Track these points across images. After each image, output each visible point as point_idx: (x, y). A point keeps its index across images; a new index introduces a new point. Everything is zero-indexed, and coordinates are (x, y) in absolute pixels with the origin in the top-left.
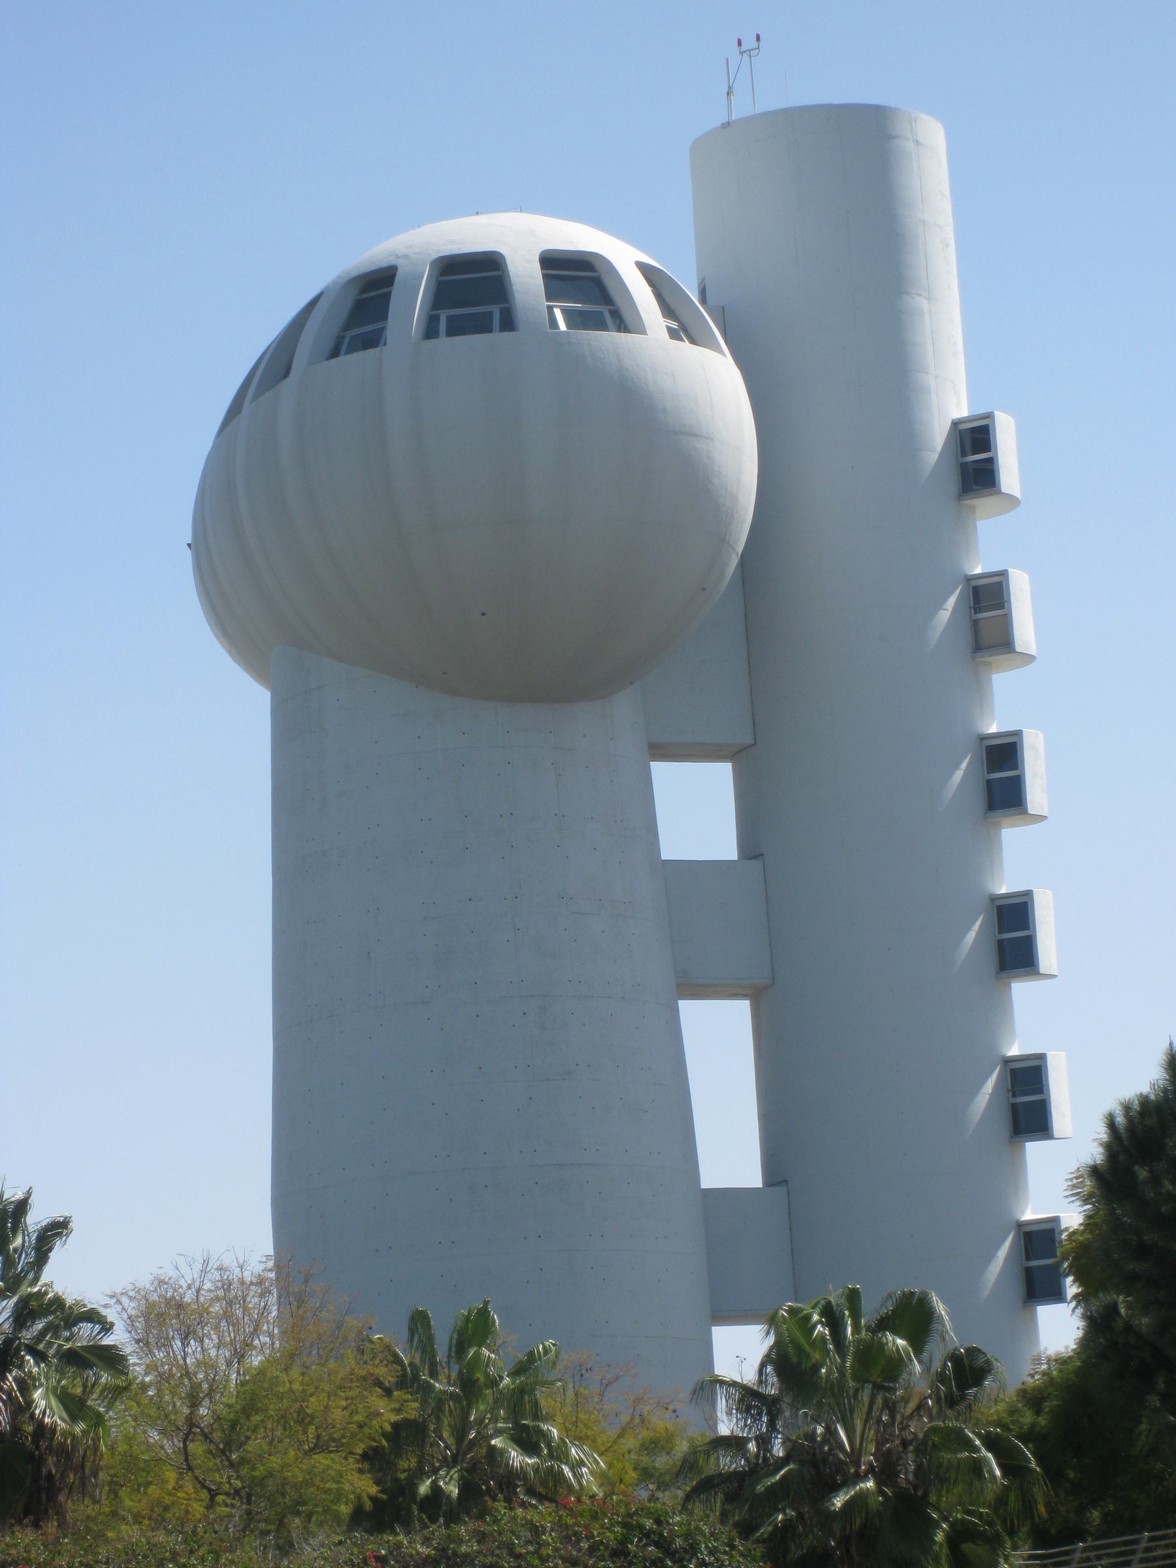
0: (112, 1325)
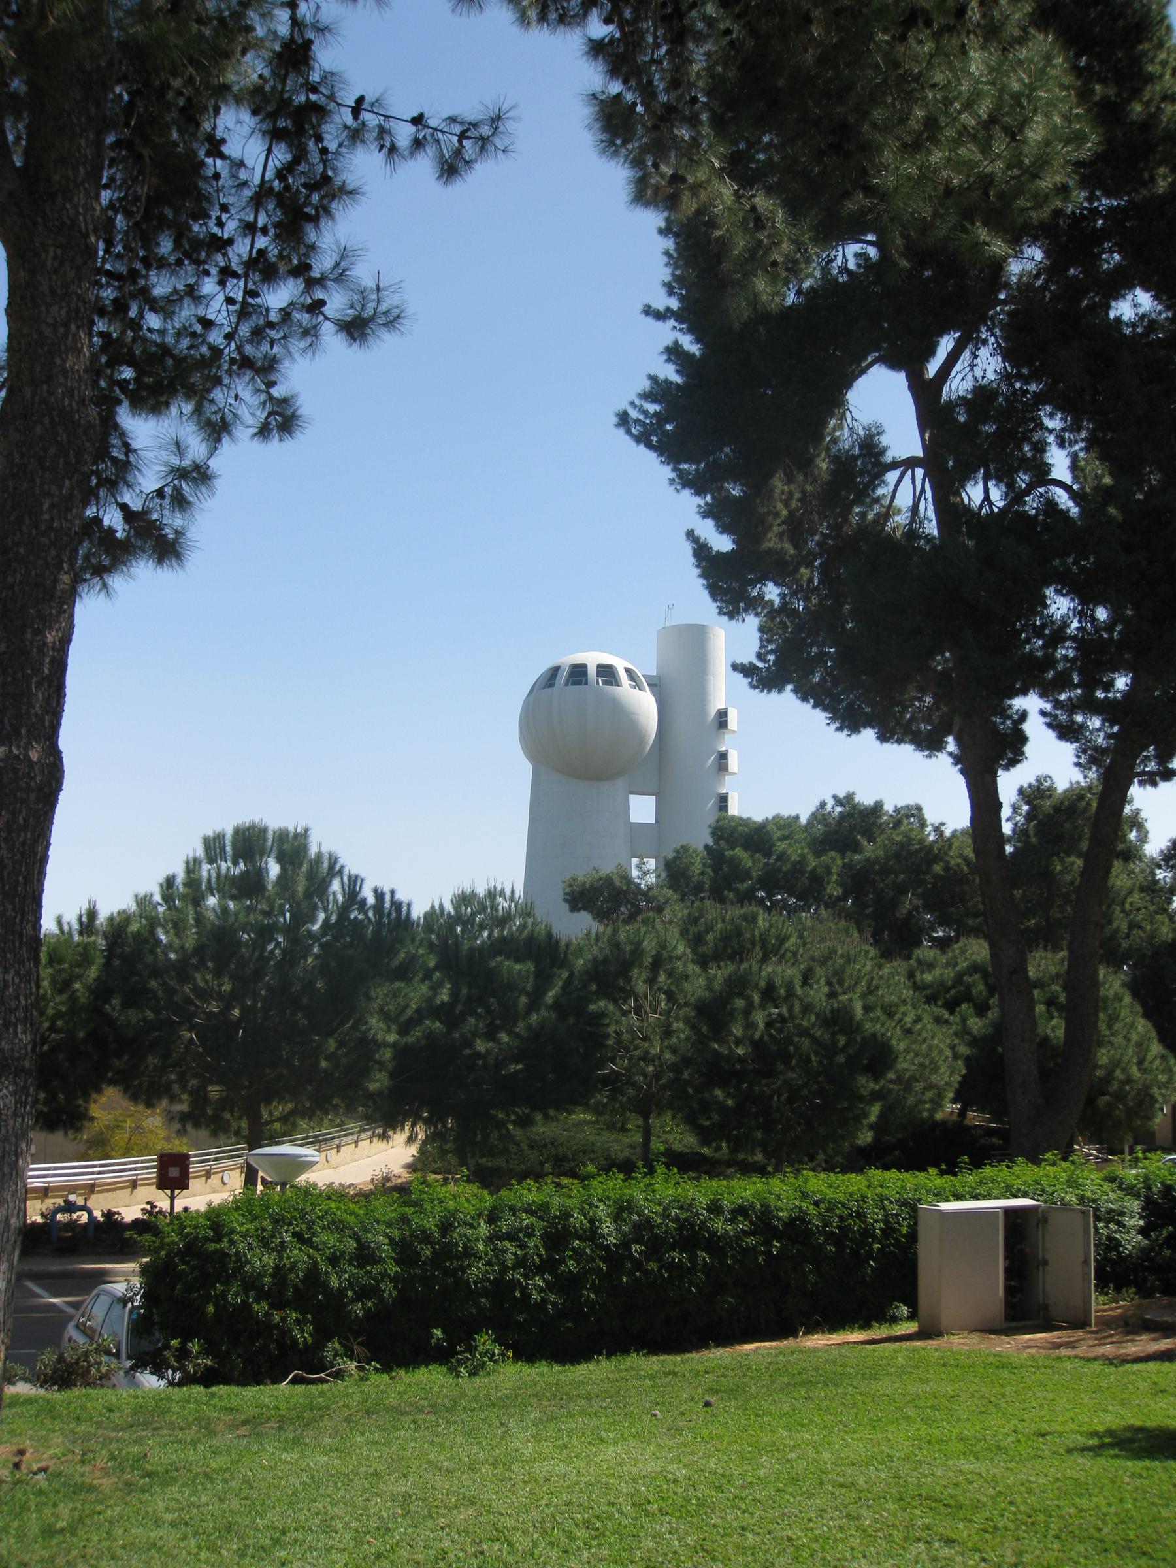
0: (574, 908)
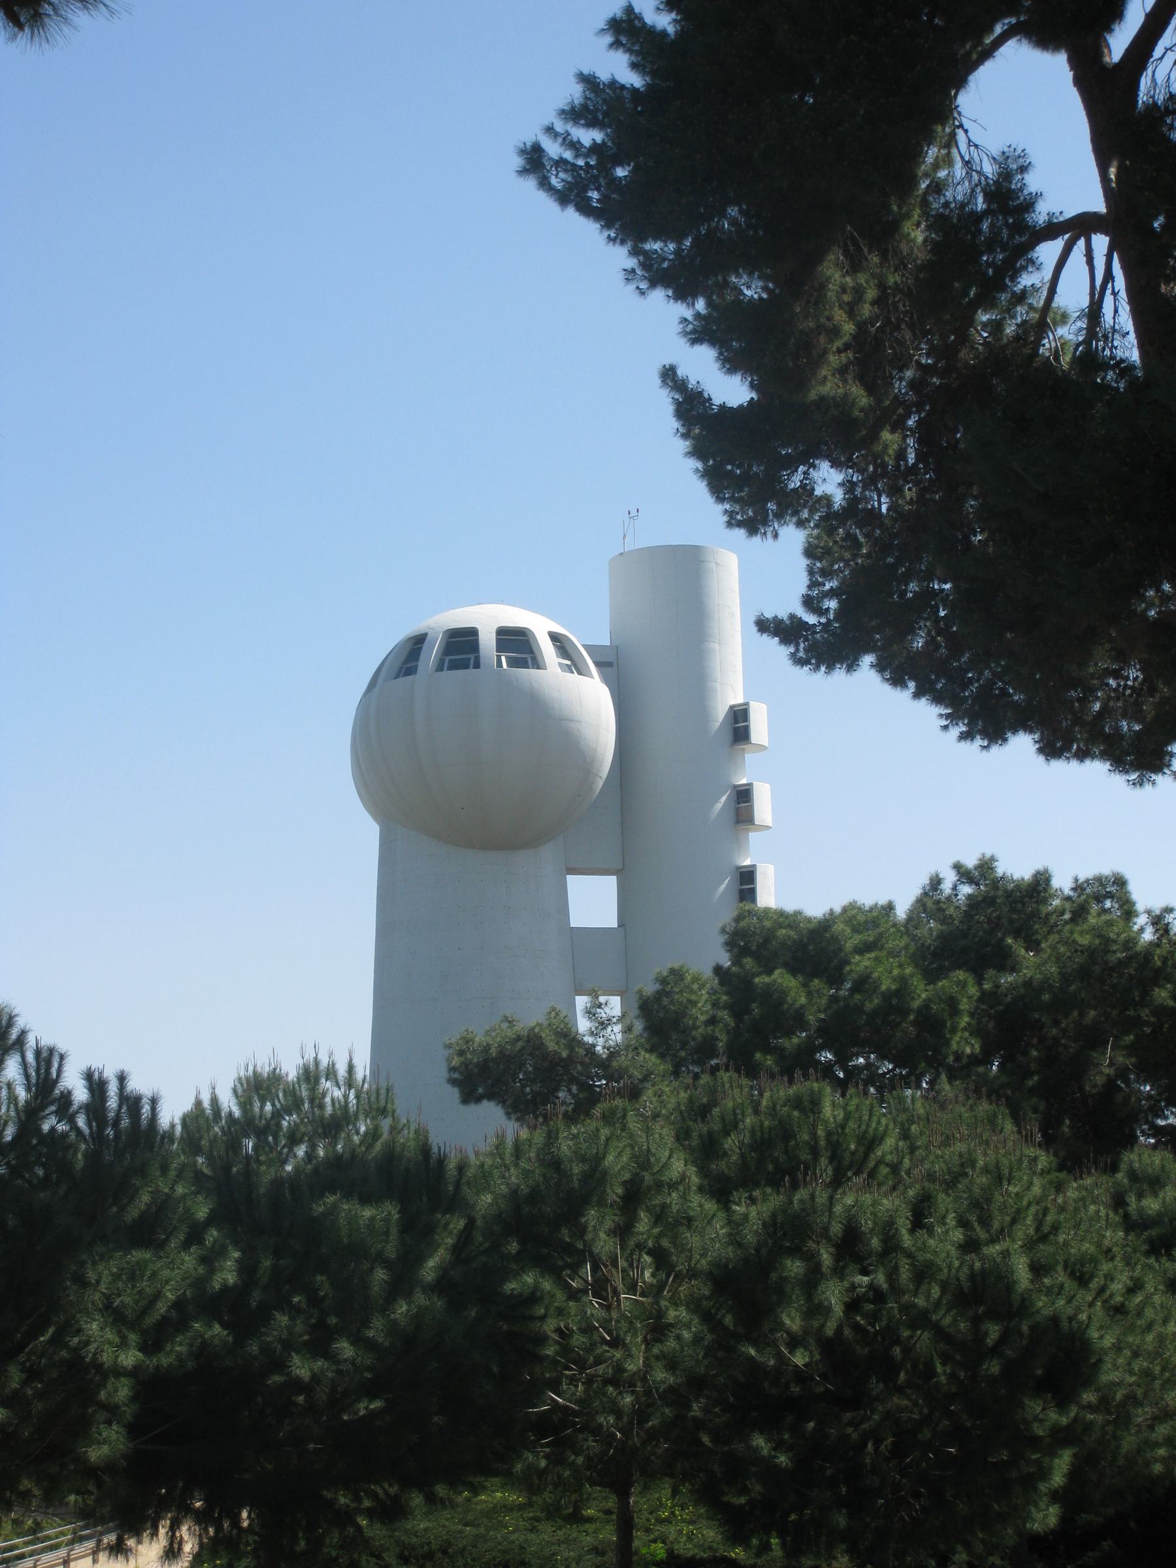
0: (469, 1097)
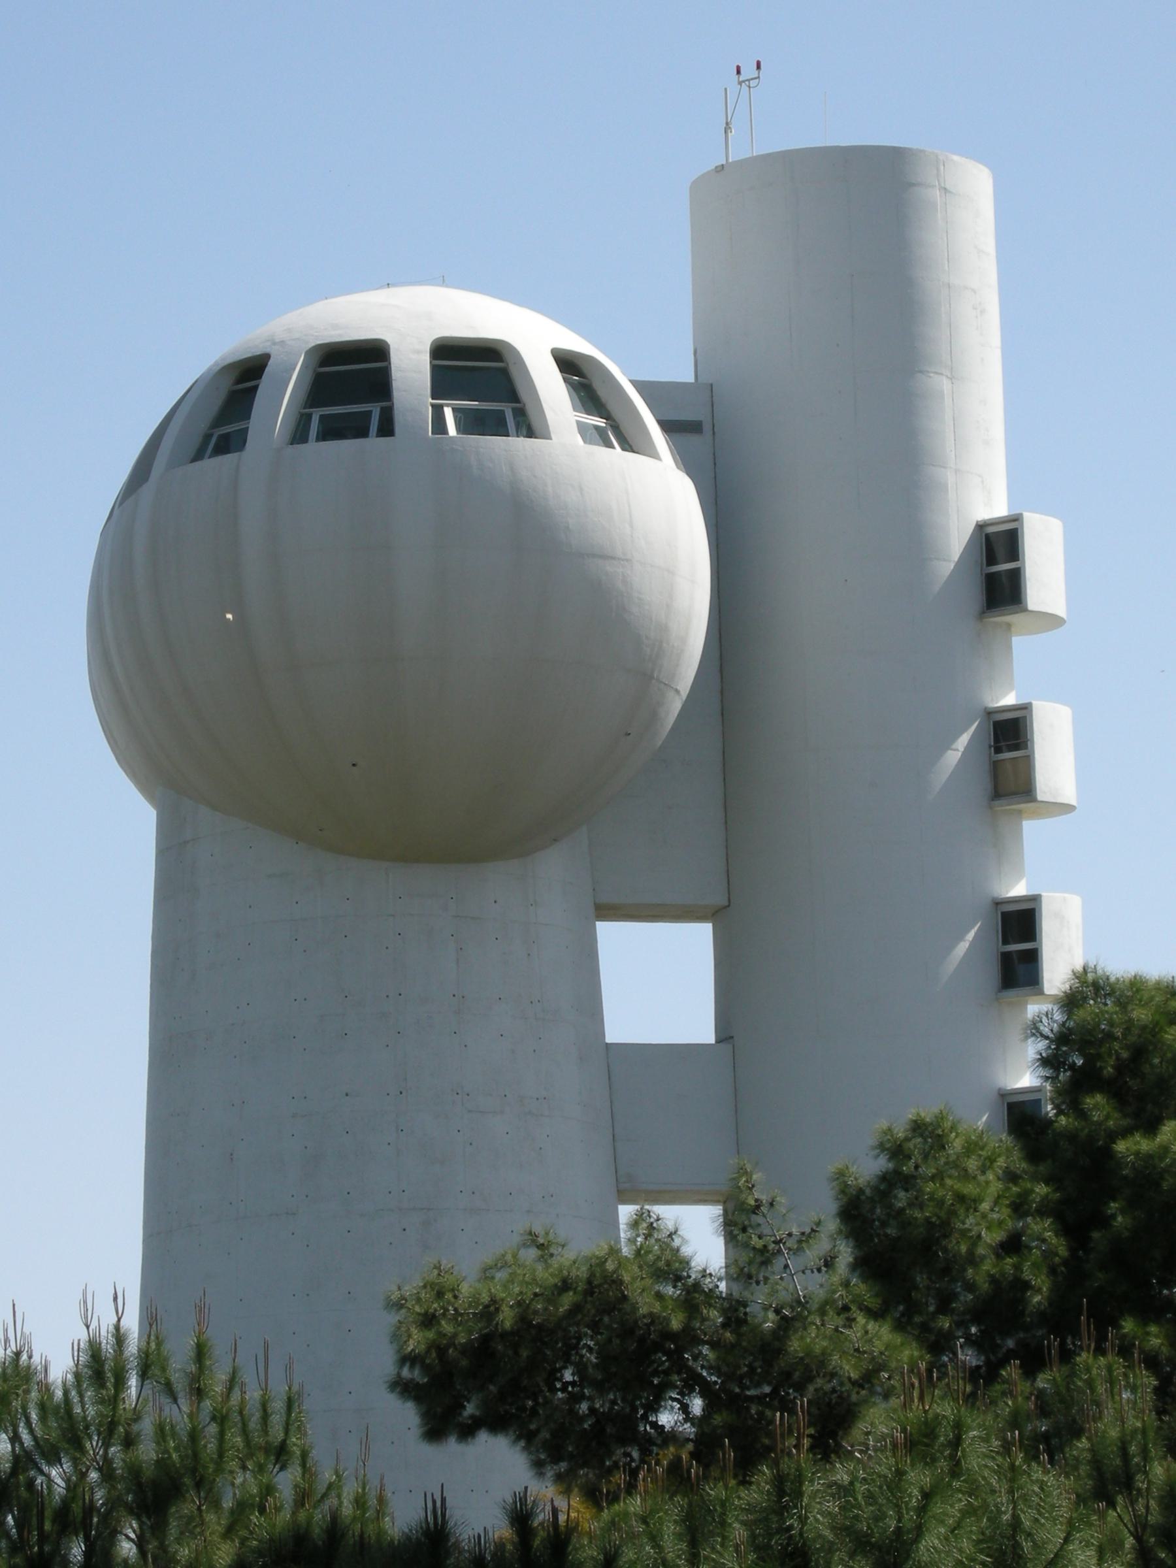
0: (442, 1421)
